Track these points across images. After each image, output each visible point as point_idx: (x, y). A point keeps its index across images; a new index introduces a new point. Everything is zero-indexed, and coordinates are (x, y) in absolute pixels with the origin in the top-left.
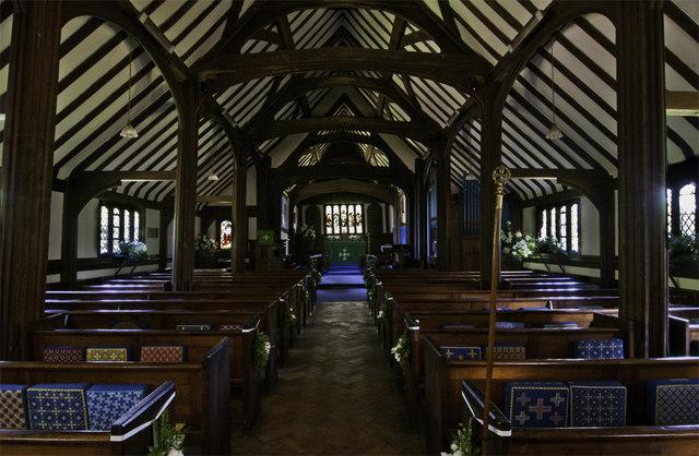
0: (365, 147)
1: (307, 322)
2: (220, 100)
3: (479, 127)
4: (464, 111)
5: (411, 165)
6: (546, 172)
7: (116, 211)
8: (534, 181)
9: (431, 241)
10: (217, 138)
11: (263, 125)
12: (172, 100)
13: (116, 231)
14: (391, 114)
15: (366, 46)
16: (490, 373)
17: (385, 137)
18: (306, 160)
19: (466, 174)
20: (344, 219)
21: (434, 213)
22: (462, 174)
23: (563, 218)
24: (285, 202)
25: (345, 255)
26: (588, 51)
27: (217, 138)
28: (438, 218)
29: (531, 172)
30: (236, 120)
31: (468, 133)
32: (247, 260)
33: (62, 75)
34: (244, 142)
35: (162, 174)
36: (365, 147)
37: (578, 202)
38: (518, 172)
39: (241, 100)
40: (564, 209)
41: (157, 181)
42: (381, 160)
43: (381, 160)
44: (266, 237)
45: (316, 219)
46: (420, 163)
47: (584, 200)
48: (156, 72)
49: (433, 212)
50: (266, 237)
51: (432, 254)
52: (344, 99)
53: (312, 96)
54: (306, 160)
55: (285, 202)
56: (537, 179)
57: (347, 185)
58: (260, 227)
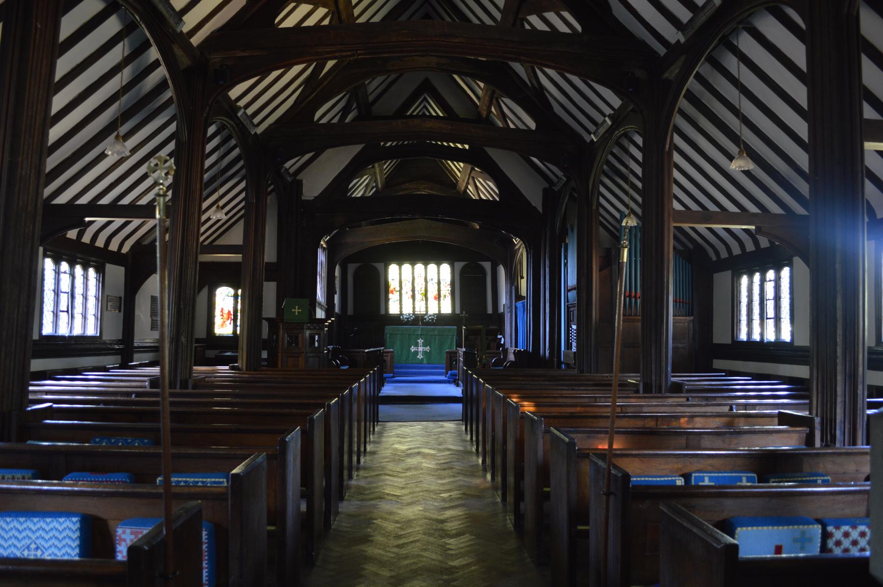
0: (458, 168)
1: (368, 448)
2: (234, 93)
3: (639, 140)
4: (618, 118)
5: (536, 199)
6: (743, 216)
7: (64, 266)
8: (693, 229)
9: (568, 327)
10: (222, 150)
11: (298, 132)
12: (169, 94)
13: (63, 306)
14: (504, 116)
15: (476, 21)
16: (611, 445)
17: (496, 154)
18: (360, 188)
19: (623, 216)
20: (420, 289)
21: (572, 280)
22: (617, 215)
23: (770, 288)
24: (322, 257)
25: (420, 349)
26: (773, 54)
27: (222, 150)
28: (578, 288)
29: (724, 216)
30: (256, 120)
31: (626, 151)
32: (265, 355)
33: (58, 75)
34: (266, 157)
35: (133, 210)
36: (458, 168)
37: (790, 265)
38: (687, 215)
39: (266, 96)
40: (771, 274)
41: (142, 220)
42: (484, 189)
43: (484, 189)
44: (297, 310)
45: (373, 289)
46: (550, 196)
47: (797, 260)
48: (154, 54)
49: (570, 276)
50: (297, 310)
51: (569, 346)
52: (426, 88)
53: (374, 85)
54: (360, 188)
55: (322, 257)
56: (696, 226)
57: (422, 228)
58: (280, 297)
